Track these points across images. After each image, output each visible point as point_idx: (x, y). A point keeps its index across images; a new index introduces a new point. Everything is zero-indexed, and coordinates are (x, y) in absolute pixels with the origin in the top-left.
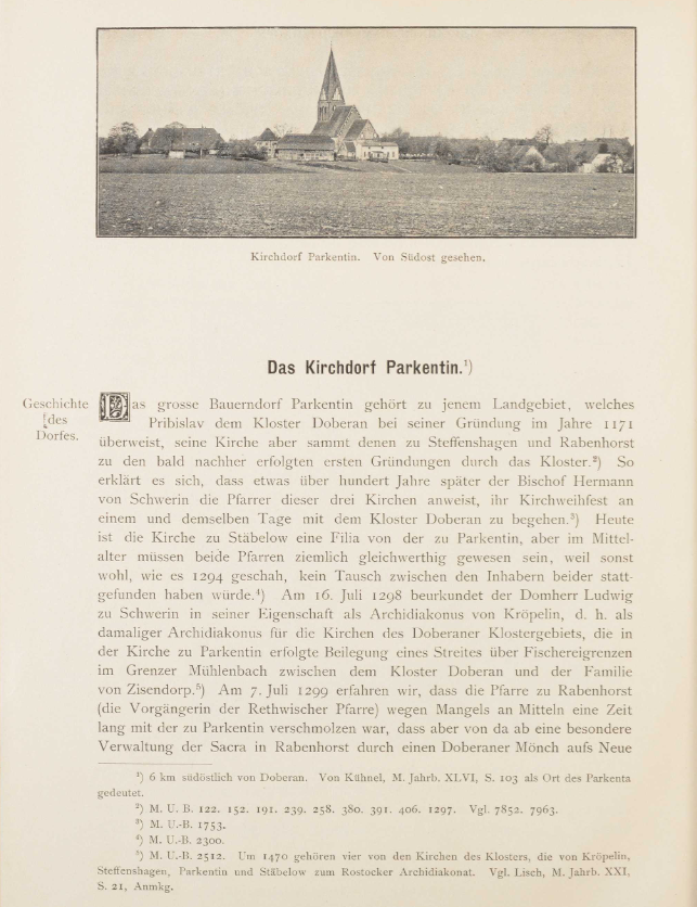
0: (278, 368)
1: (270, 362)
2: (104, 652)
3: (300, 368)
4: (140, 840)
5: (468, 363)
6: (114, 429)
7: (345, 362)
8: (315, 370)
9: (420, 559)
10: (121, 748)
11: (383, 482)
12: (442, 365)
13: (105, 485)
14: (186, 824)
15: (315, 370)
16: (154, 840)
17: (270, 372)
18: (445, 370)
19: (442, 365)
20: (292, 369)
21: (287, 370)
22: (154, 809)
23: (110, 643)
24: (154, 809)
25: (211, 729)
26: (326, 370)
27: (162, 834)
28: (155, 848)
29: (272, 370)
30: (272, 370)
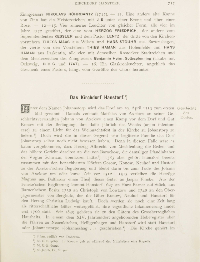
0: (73, 98)
1: (71, 96)
2: (23, 201)
3: (79, 98)
4: (34, 250)
5: (126, 96)
6: (26, 115)
7: (92, 96)
8: (84, 98)
9: (36, 48)
10: (43, 120)
11: (166, 228)
12: (116, 97)
13: (69, 21)
14: (47, 246)
15: (84, 98)
16: (39, 245)
17: (71, 99)
18: (116, 98)
19: (116, 97)
20: (77, 98)
21: (76, 98)
22: (38, 250)
23: (170, 34)
24: (38, 250)
25: (49, 53)
26: (87, 98)
27: (41, 243)
28: (39, 243)
29: (71, 98)
30: (71, 98)
